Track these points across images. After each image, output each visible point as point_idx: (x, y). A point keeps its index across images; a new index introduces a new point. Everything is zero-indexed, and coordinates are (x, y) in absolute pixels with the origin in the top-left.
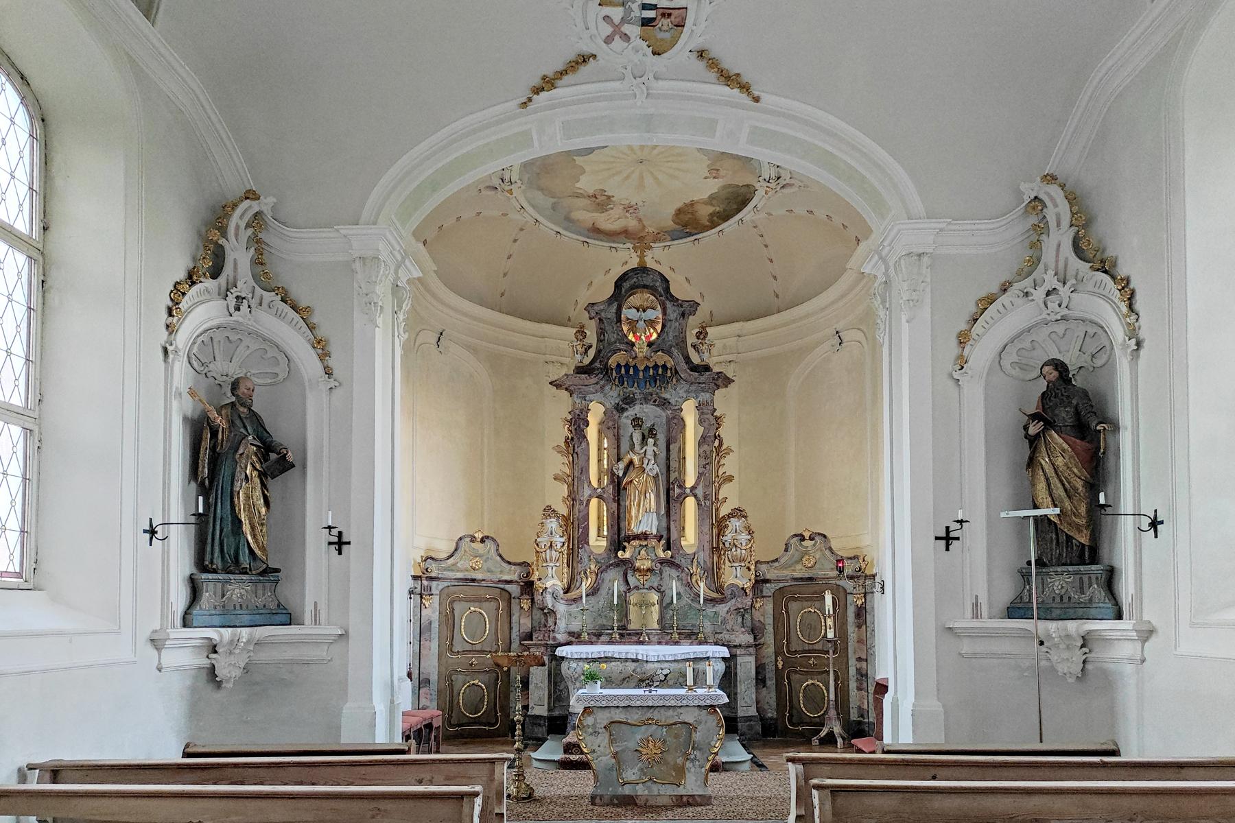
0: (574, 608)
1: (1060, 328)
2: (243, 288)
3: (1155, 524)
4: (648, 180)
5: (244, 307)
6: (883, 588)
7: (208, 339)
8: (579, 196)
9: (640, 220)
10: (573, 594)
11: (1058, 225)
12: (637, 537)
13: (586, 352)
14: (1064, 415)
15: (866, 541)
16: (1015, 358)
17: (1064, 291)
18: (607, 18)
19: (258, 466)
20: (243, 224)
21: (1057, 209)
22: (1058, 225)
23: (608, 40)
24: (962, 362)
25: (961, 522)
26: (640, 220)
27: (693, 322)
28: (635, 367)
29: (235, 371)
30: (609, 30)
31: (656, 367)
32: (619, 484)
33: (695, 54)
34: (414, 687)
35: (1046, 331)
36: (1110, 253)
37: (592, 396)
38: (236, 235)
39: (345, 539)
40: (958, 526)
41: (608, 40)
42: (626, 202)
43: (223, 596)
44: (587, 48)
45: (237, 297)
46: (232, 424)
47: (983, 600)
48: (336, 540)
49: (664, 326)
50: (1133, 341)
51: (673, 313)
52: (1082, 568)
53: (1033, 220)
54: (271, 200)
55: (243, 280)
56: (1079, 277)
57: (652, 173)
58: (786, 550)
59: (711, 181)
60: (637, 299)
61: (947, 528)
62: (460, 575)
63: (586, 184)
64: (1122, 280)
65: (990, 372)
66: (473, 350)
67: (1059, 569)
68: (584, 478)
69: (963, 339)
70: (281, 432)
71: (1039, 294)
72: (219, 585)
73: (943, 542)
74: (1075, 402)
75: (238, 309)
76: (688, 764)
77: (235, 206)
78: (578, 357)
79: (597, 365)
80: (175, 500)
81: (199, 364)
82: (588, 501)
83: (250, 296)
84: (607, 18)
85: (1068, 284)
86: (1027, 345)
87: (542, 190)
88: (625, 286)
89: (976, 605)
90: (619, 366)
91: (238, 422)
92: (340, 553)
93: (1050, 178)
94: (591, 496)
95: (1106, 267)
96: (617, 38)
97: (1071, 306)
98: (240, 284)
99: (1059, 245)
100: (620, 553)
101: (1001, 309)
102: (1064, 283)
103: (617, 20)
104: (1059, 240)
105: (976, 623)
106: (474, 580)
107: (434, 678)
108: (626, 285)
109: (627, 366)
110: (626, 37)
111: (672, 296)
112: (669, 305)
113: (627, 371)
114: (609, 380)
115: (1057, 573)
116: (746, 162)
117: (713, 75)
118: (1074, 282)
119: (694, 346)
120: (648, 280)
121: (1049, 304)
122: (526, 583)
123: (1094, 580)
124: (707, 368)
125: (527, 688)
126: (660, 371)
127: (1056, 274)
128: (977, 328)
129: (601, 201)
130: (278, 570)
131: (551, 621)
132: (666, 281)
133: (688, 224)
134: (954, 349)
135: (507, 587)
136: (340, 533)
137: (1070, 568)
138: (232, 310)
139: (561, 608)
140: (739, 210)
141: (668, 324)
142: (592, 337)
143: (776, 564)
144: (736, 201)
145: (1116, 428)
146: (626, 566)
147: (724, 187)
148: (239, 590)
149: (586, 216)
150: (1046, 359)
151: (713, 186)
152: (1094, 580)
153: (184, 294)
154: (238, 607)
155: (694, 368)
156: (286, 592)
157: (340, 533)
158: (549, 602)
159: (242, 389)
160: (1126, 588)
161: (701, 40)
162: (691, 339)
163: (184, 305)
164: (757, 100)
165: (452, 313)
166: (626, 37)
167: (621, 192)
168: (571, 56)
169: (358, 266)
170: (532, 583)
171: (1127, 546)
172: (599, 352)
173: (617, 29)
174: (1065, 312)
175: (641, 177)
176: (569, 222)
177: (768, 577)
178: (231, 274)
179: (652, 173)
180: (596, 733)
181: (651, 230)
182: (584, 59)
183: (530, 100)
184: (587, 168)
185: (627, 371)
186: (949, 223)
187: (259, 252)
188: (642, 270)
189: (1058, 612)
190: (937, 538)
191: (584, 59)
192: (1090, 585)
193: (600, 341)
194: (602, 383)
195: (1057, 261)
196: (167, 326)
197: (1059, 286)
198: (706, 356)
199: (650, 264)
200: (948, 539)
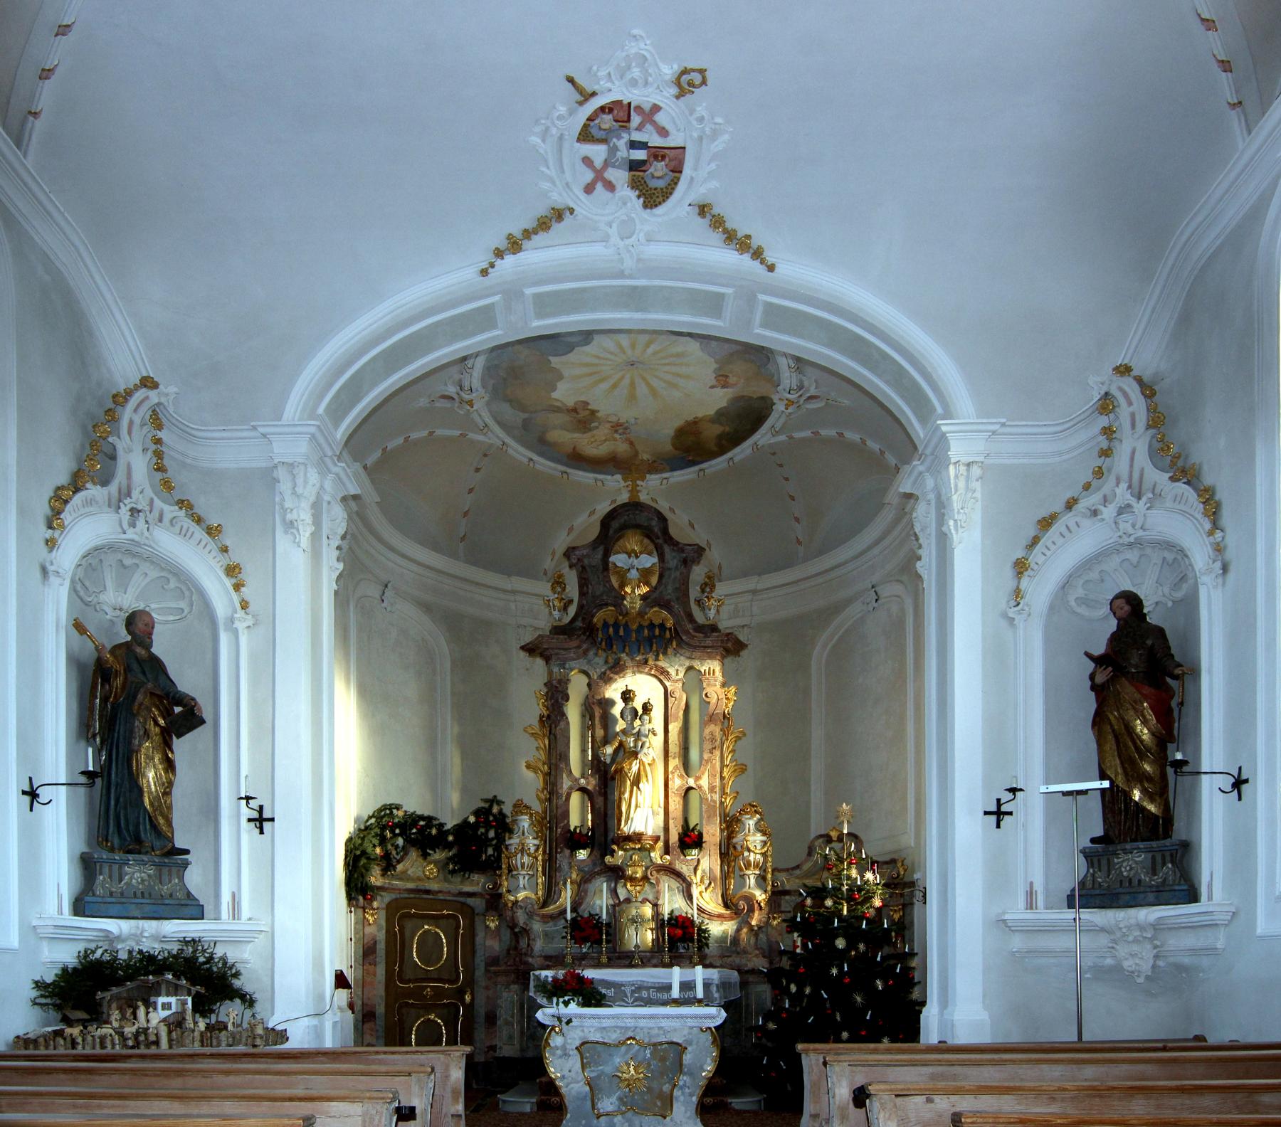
0: (550, 927)
1: (1133, 556)
2: (139, 498)
3: (1239, 783)
4: (642, 390)
5: (141, 523)
6: (924, 896)
7: (93, 559)
8: (557, 410)
9: (631, 443)
10: (551, 909)
11: (1133, 426)
12: (628, 838)
13: (565, 608)
14: (1135, 659)
15: (909, 840)
16: (1080, 592)
17: (1140, 507)
18: (587, 161)
19: (162, 722)
20: (137, 420)
21: (1133, 407)
22: (1133, 426)
23: (589, 189)
24: (1017, 594)
25: (1013, 790)
26: (631, 443)
27: (698, 573)
28: (626, 626)
29: (131, 601)
30: (589, 176)
31: (652, 626)
32: (606, 772)
33: (697, 210)
34: (356, 1020)
35: (1116, 559)
36: (1195, 458)
37: (572, 664)
38: (130, 432)
39: (266, 815)
40: (1011, 796)
41: (589, 189)
42: (614, 419)
43: (121, 881)
44: (559, 198)
45: (132, 510)
46: (128, 669)
47: (1039, 887)
48: (256, 815)
49: (661, 577)
50: (1218, 564)
51: (672, 559)
52: (1154, 844)
53: (1103, 421)
54: (172, 389)
55: (139, 490)
56: (1157, 491)
57: (644, 379)
58: (810, 854)
59: (719, 392)
60: (633, 541)
61: (998, 800)
62: (411, 885)
63: (564, 393)
64: (1206, 490)
65: (1052, 608)
66: (427, 608)
67: (1128, 846)
68: (563, 765)
69: (1020, 567)
70: (185, 680)
71: (1108, 512)
72: (116, 867)
73: (994, 818)
74: (1149, 642)
75: (133, 525)
76: (676, 1093)
77: (129, 393)
78: (556, 614)
79: (579, 624)
80: (58, 752)
81: (82, 589)
82: (569, 795)
83: (147, 508)
84: (587, 161)
85: (1144, 499)
86: (1094, 575)
87: (510, 401)
88: (617, 524)
89: (1031, 894)
90: (606, 625)
91: (135, 666)
92: (262, 832)
93: (1123, 370)
94: (571, 788)
95: (1185, 473)
96: (599, 186)
97: (1146, 527)
98: (135, 494)
99: (1133, 453)
100: (608, 859)
101: (1063, 529)
102: (1139, 498)
103: (598, 163)
104: (1134, 444)
105: (1029, 915)
106: (428, 892)
107: (381, 1010)
108: (615, 525)
109: (616, 625)
110: (610, 187)
111: (671, 538)
112: (667, 549)
113: (616, 631)
114: (594, 643)
115: (1125, 851)
116: (758, 356)
117: (717, 237)
118: (1150, 495)
119: (699, 602)
120: (642, 519)
121: (1122, 526)
122: (492, 896)
123: (1168, 858)
124: (714, 628)
125: (494, 1023)
126: (657, 632)
127: (1130, 487)
128: (1036, 556)
129: (583, 417)
130: (187, 852)
131: (523, 943)
132: (662, 519)
133: (691, 447)
134: (1011, 584)
135: (470, 901)
136: (261, 807)
137: (1141, 845)
138: (126, 526)
139: (537, 927)
140: (753, 430)
141: (667, 573)
142: (573, 590)
143: (798, 872)
144: (747, 417)
145: (1195, 672)
146: (617, 874)
147: (737, 400)
148: (137, 874)
149: (563, 437)
150: (1117, 591)
151: (719, 399)
152: (1168, 858)
153: (66, 502)
154: (139, 894)
155: (700, 629)
156: (194, 879)
157: (261, 807)
158: (521, 917)
159: (140, 625)
160: (1212, 862)
161: (703, 190)
162: (694, 592)
163: (67, 516)
164: (771, 268)
165: (399, 560)
166: (610, 187)
167: (607, 404)
168: (542, 210)
169: (281, 473)
170: (500, 896)
171: (1212, 819)
172: (581, 607)
173: (599, 176)
174: (1140, 533)
175: (632, 384)
176: (542, 445)
177: (787, 887)
178: (124, 483)
179: (644, 379)
180: (566, 1055)
181: (646, 457)
182: (559, 214)
183: (492, 265)
184: (566, 373)
185: (616, 631)
186: (1003, 425)
187: (159, 455)
188: (634, 506)
189: (1127, 897)
190: (986, 813)
191: (559, 214)
192: (1164, 864)
193: (582, 594)
194: (585, 646)
195: (1131, 472)
196: (47, 541)
197: (1133, 501)
198: (712, 613)
199: (643, 498)
200: (999, 814)
